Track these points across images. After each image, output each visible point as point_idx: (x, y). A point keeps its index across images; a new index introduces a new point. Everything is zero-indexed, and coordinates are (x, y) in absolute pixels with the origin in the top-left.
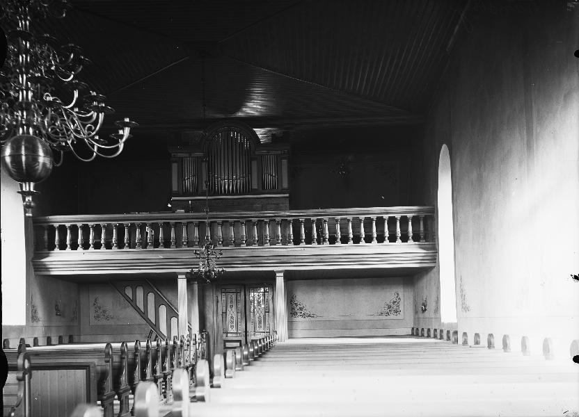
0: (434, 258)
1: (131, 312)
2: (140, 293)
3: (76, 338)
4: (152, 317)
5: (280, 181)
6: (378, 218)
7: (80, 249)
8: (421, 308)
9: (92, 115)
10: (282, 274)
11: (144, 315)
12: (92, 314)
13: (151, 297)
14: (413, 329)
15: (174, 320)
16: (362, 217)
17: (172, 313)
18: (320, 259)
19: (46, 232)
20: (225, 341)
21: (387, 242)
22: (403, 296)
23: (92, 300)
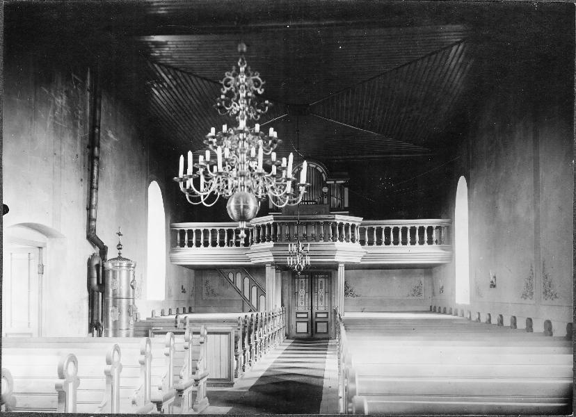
0: (451, 258)
1: (231, 289)
2: (239, 277)
3: (193, 310)
4: (247, 295)
5: (343, 202)
6: (420, 227)
7: (218, 247)
8: (437, 291)
9: (270, 155)
10: (343, 265)
11: (241, 293)
12: (204, 292)
13: (247, 280)
14: (431, 307)
15: (262, 297)
16: (367, 227)
17: (262, 292)
18: (383, 256)
19: (179, 234)
20: (297, 313)
21: (392, 245)
22: (421, 279)
23: (204, 282)
